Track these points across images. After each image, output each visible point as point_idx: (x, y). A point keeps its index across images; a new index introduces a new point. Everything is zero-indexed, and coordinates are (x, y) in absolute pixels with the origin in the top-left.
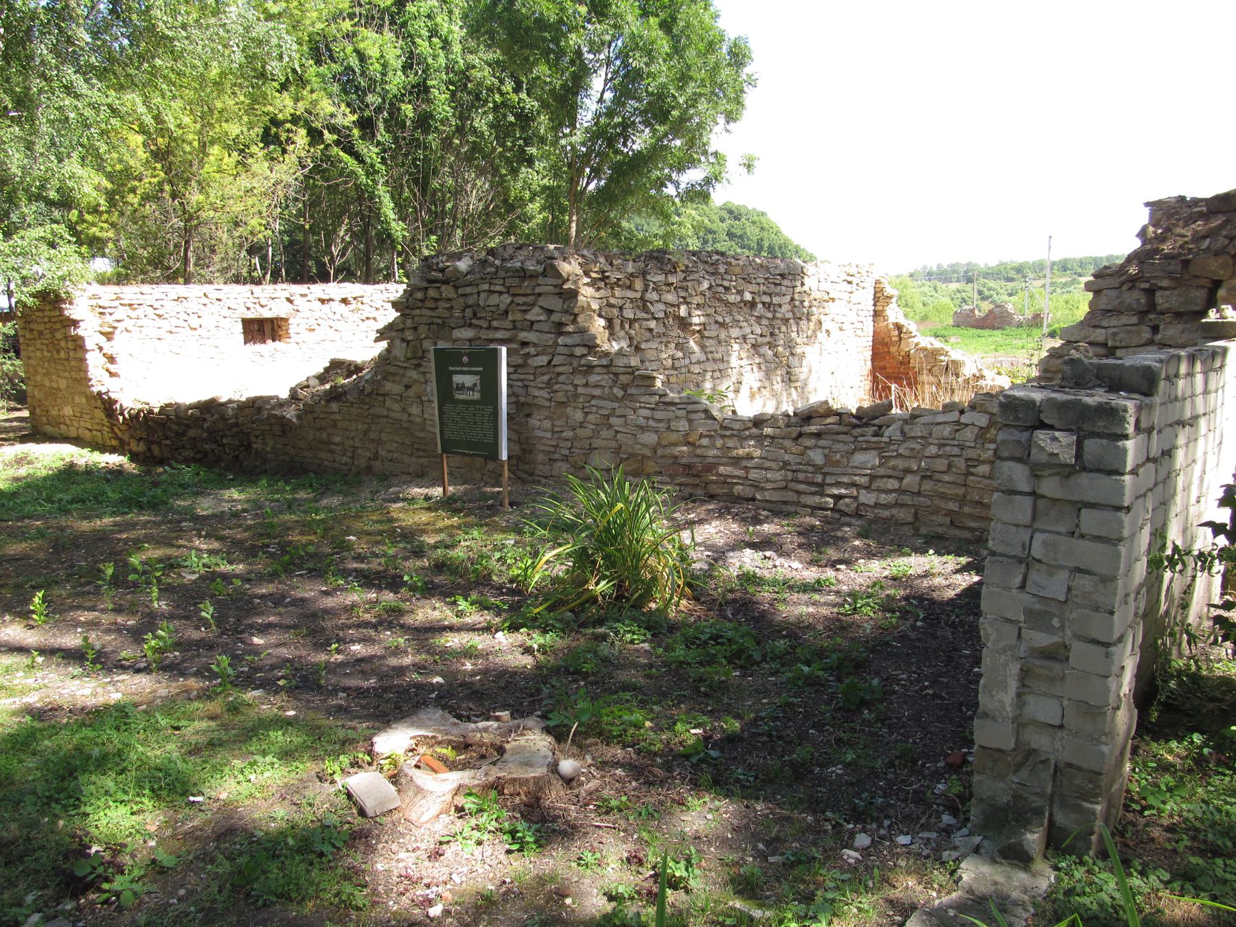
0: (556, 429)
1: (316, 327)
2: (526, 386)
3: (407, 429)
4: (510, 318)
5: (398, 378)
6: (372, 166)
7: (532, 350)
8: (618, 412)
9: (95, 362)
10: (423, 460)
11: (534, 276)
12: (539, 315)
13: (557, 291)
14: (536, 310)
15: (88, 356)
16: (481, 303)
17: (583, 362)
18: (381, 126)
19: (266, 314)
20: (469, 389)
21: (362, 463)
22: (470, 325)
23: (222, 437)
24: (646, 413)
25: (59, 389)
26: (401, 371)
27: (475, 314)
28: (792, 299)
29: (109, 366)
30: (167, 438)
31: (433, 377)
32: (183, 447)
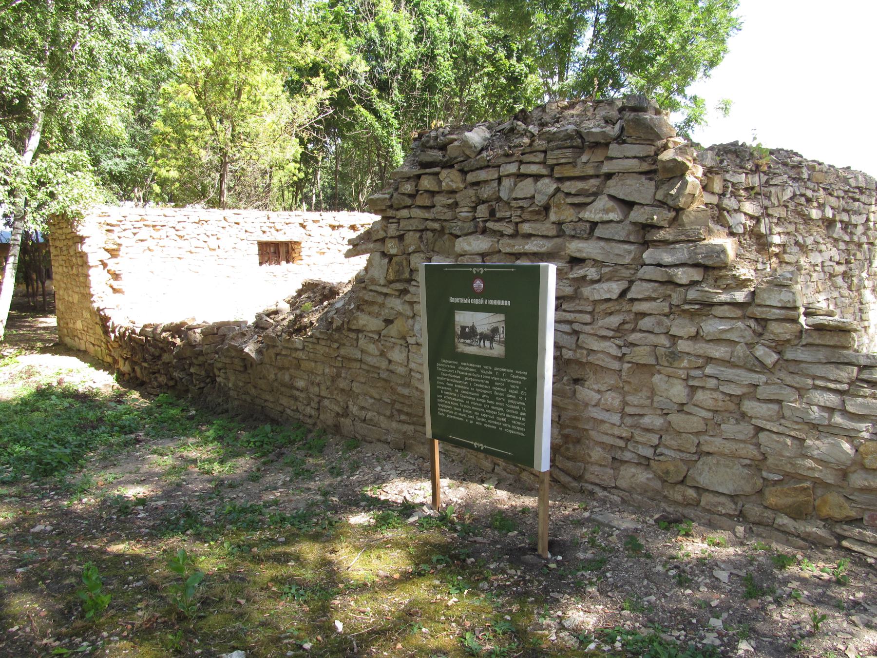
0: (628, 410)
1: (326, 250)
2: (576, 333)
3: (386, 381)
4: (553, 217)
5: (376, 309)
6: (387, 120)
7: (592, 273)
8: (764, 392)
9: (98, 279)
10: (405, 428)
11: (600, 144)
12: (607, 211)
13: (645, 167)
14: (603, 202)
15: (91, 272)
16: (504, 195)
17: (692, 294)
18: (395, 85)
19: (280, 237)
20: (484, 337)
21: (328, 418)
22: (484, 231)
23: (190, 365)
24: (832, 399)
25: (73, 303)
26: (380, 299)
27: (492, 213)
28: (868, 220)
29: (112, 282)
30: (145, 360)
31: (422, 308)
32: (159, 372)
